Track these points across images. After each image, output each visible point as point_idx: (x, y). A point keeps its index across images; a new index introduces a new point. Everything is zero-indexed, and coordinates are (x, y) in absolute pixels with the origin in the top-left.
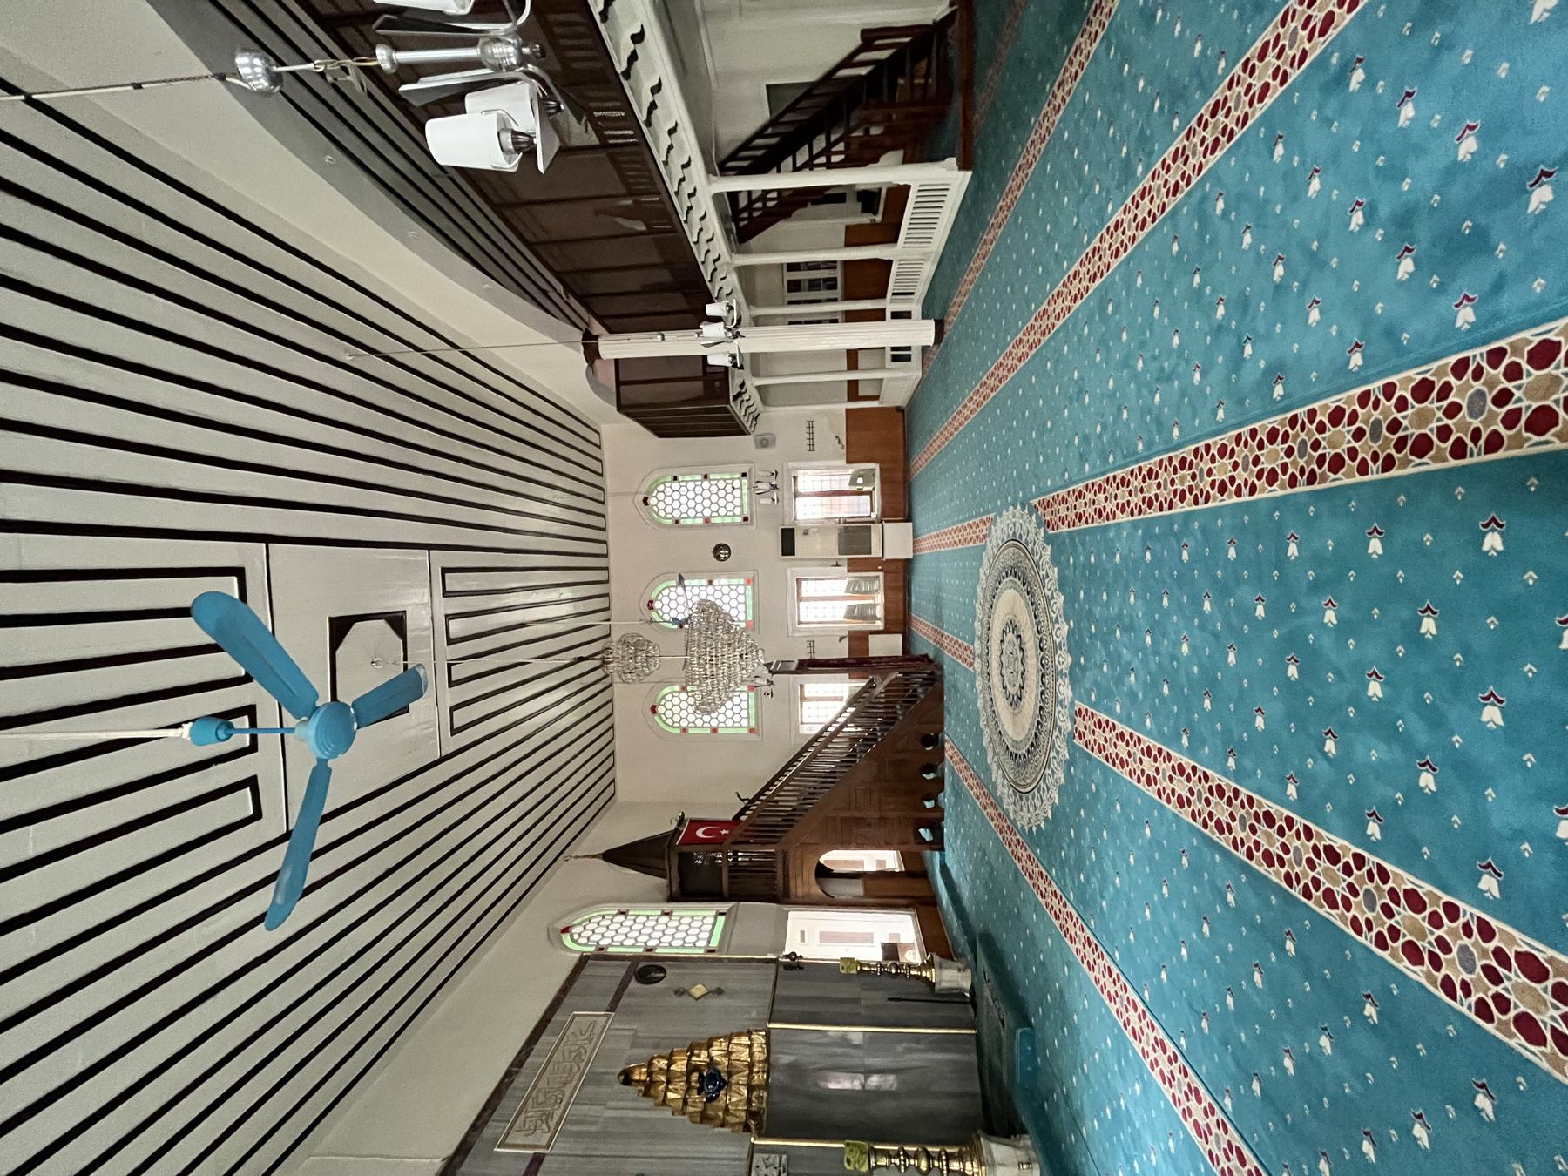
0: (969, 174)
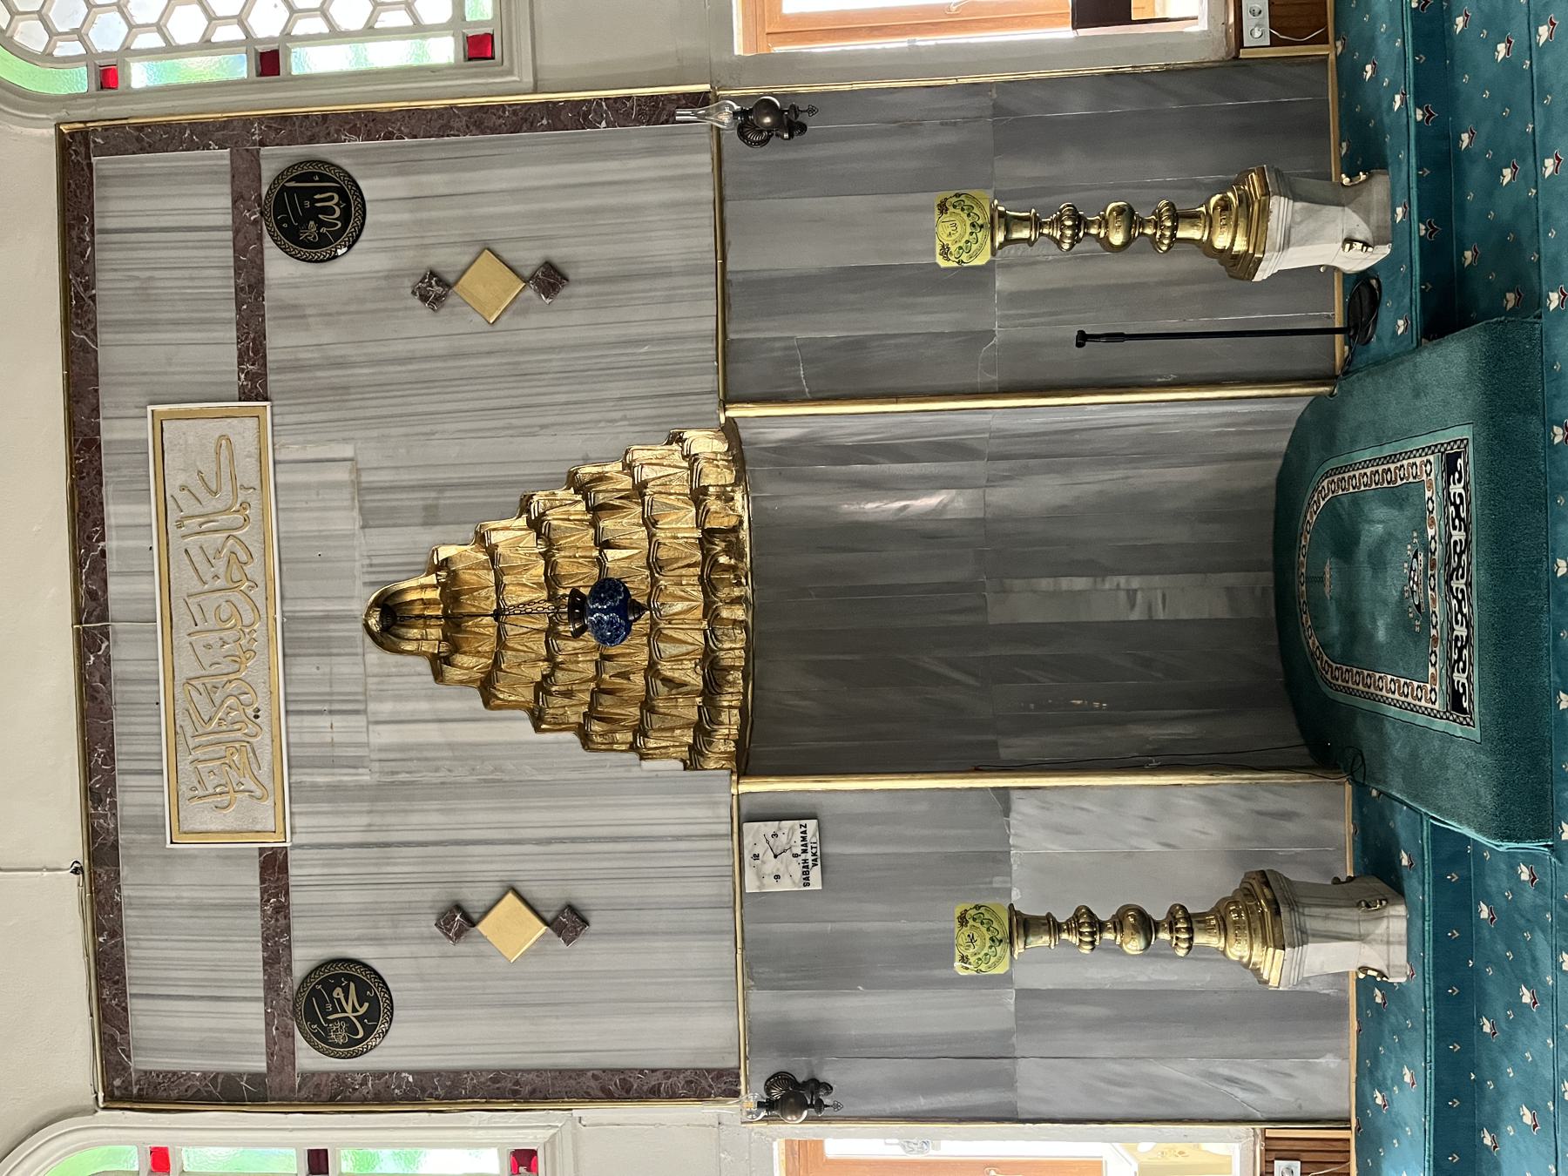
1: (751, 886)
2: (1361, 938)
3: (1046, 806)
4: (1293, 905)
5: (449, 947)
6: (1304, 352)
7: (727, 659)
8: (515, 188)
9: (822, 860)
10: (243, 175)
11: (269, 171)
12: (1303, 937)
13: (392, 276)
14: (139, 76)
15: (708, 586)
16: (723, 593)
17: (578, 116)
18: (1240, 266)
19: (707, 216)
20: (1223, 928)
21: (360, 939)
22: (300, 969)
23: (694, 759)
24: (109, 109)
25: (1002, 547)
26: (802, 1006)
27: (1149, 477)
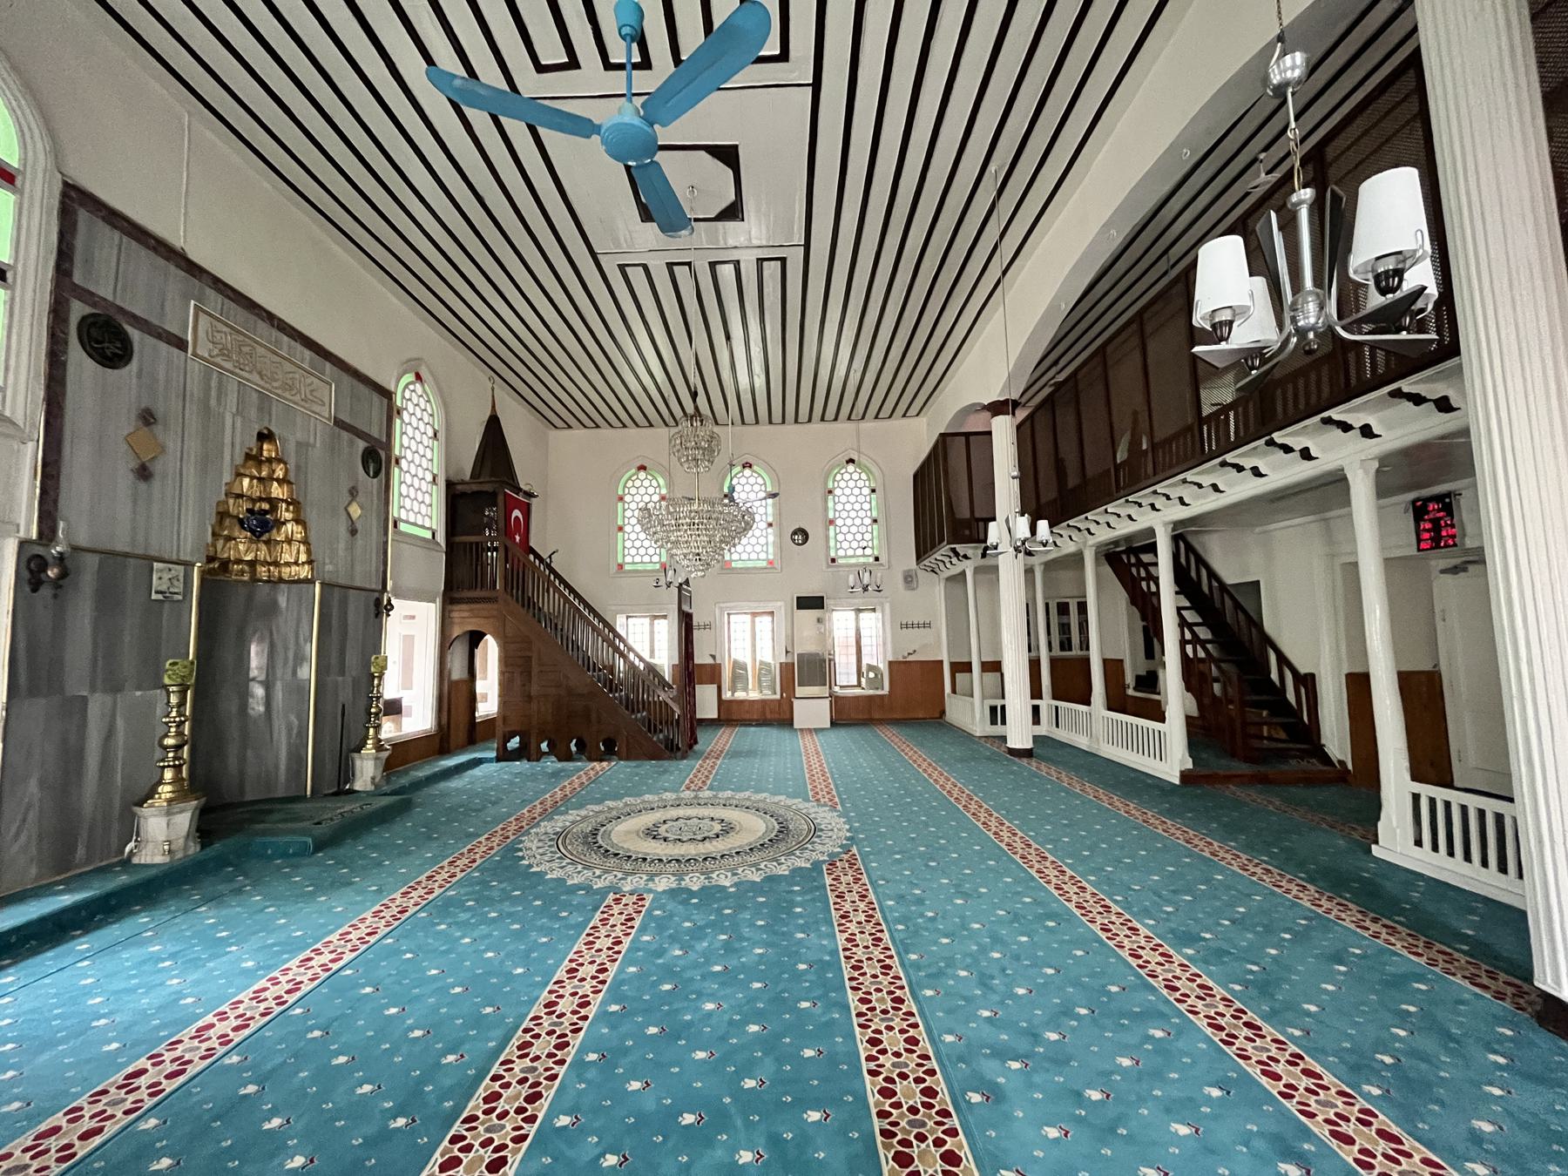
0: (1177, 782)
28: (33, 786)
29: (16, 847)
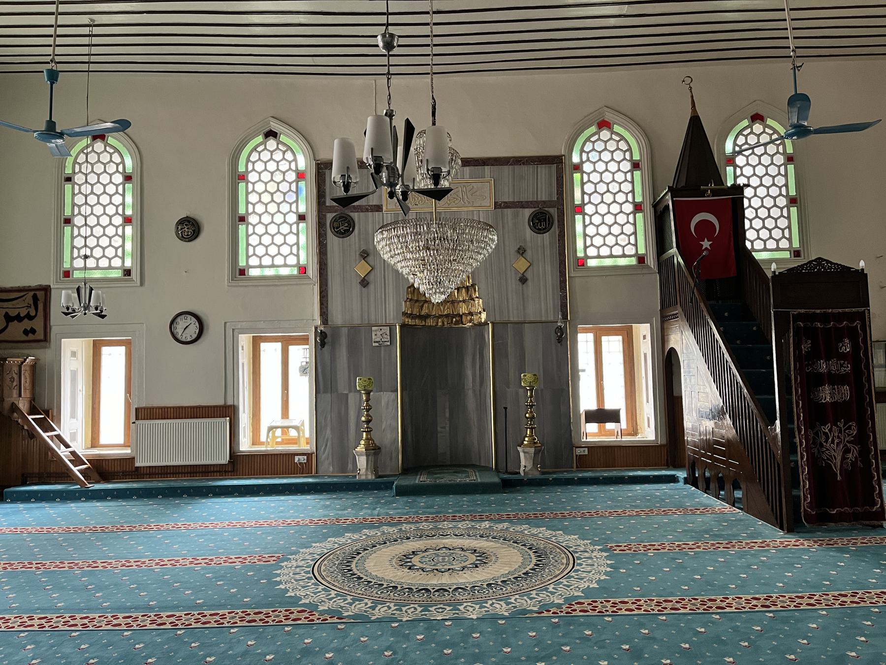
1: (373, 328)
2: (367, 468)
3: (393, 400)
4: (375, 453)
5: (358, 253)
6: (502, 465)
7: (428, 321)
8: (546, 271)
9: (380, 346)
10: (551, 204)
11: (551, 210)
12: (367, 456)
13: (525, 241)
14: (577, 176)
15: (447, 316)
16: (445, 320)
17: (563, 288)
18: (521, 444)
19: (538, 319)
20: (367, 439)
21: (360, 230)
22: (352, 214)
23: (404, 314)
24: (567, 170)
25: (457, 393)
26: (344, 340)
27: (475, 432)
28: (328, 432)
29: (324, 456)
